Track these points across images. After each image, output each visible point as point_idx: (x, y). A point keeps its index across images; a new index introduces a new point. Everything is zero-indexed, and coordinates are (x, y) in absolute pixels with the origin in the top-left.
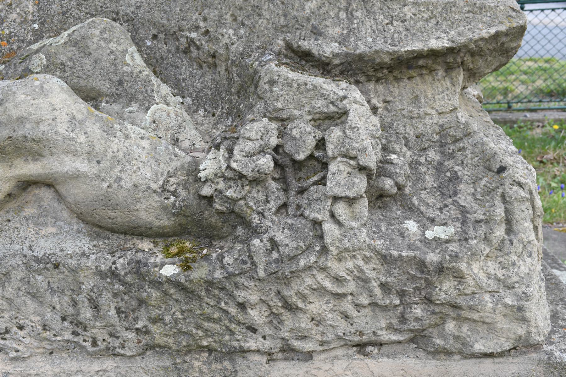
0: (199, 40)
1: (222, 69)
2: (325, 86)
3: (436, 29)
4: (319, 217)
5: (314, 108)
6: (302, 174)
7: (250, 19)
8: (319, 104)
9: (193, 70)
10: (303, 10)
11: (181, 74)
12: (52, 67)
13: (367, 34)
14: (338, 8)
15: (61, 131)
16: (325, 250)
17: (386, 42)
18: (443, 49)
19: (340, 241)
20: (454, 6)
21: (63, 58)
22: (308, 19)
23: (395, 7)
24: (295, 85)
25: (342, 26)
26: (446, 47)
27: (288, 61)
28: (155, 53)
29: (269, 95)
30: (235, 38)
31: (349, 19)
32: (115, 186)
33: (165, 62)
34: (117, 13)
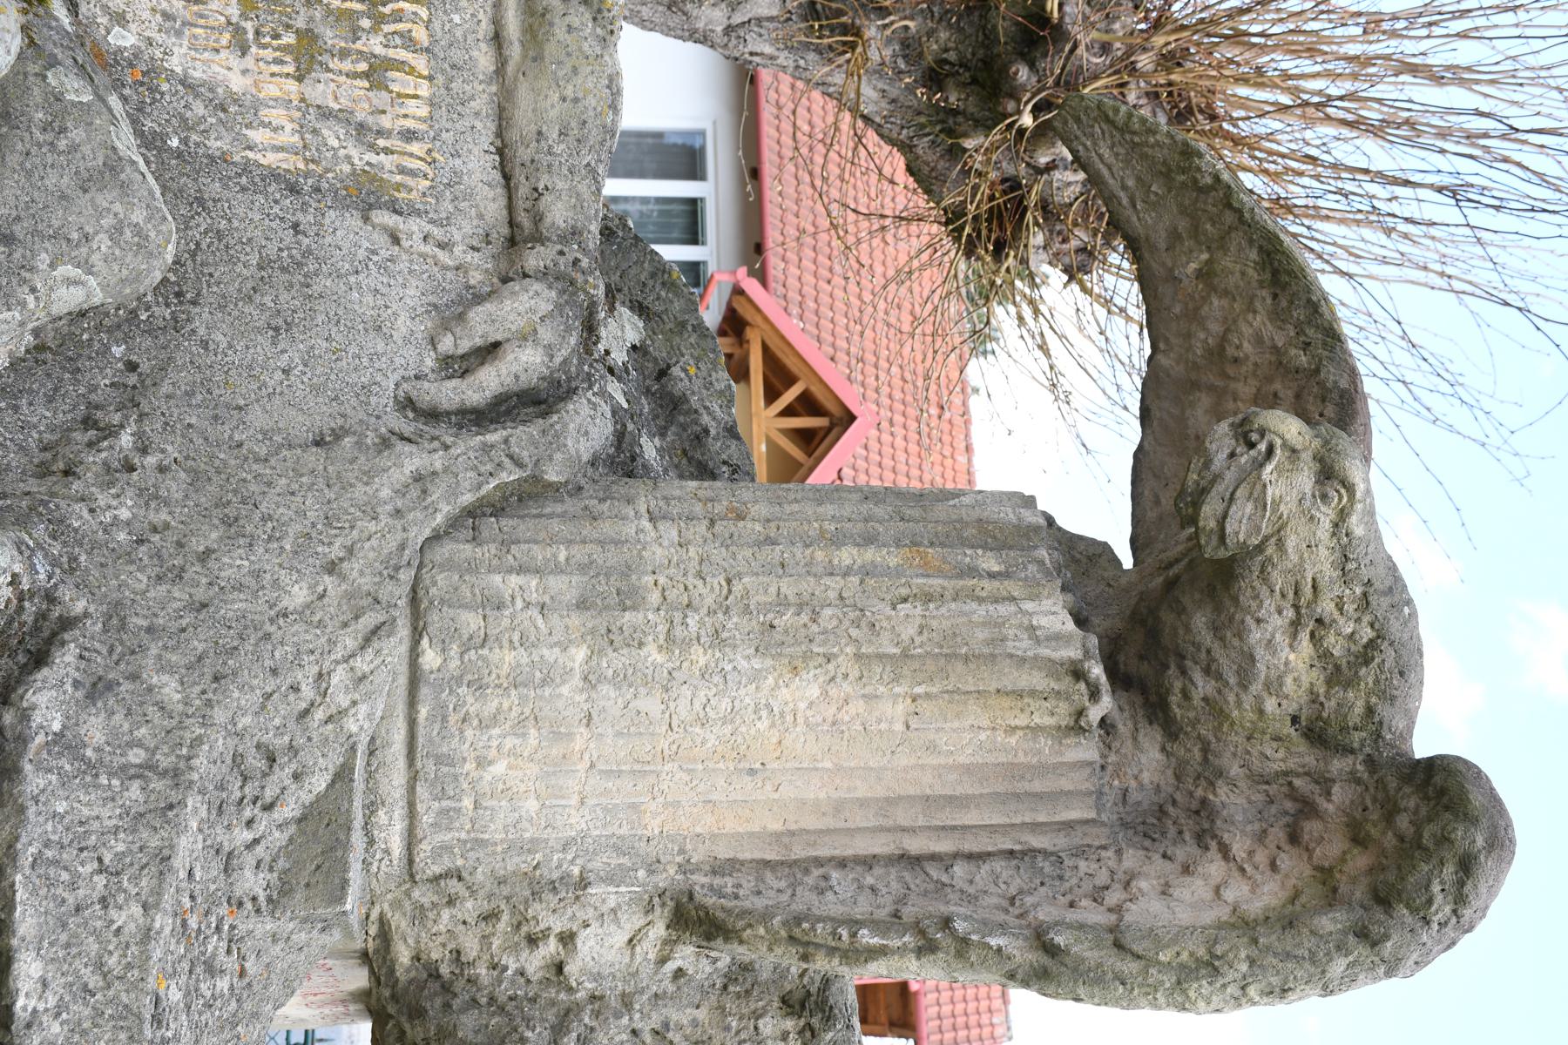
0: (111, 447)
1: (32, 485)
3: (71, 985)
7: (151, 557)
9: (40, 433)
10: (161, 670)
11: (31, 404)
12: (57, 107)
13: (75, 805)
14: (157, 748)
17: (47, 844)
18: (9, 993)
20: (131, 1038)
21: (77, 134)
22: (134, 677)
23: (144, 883)
25: (108, 749)
26: (13, 1003)
27: (28, 617)
28: (90, 358)
30: (107, 518)
31: (124, 768)
33: (67, 375)
34: (194, 303)
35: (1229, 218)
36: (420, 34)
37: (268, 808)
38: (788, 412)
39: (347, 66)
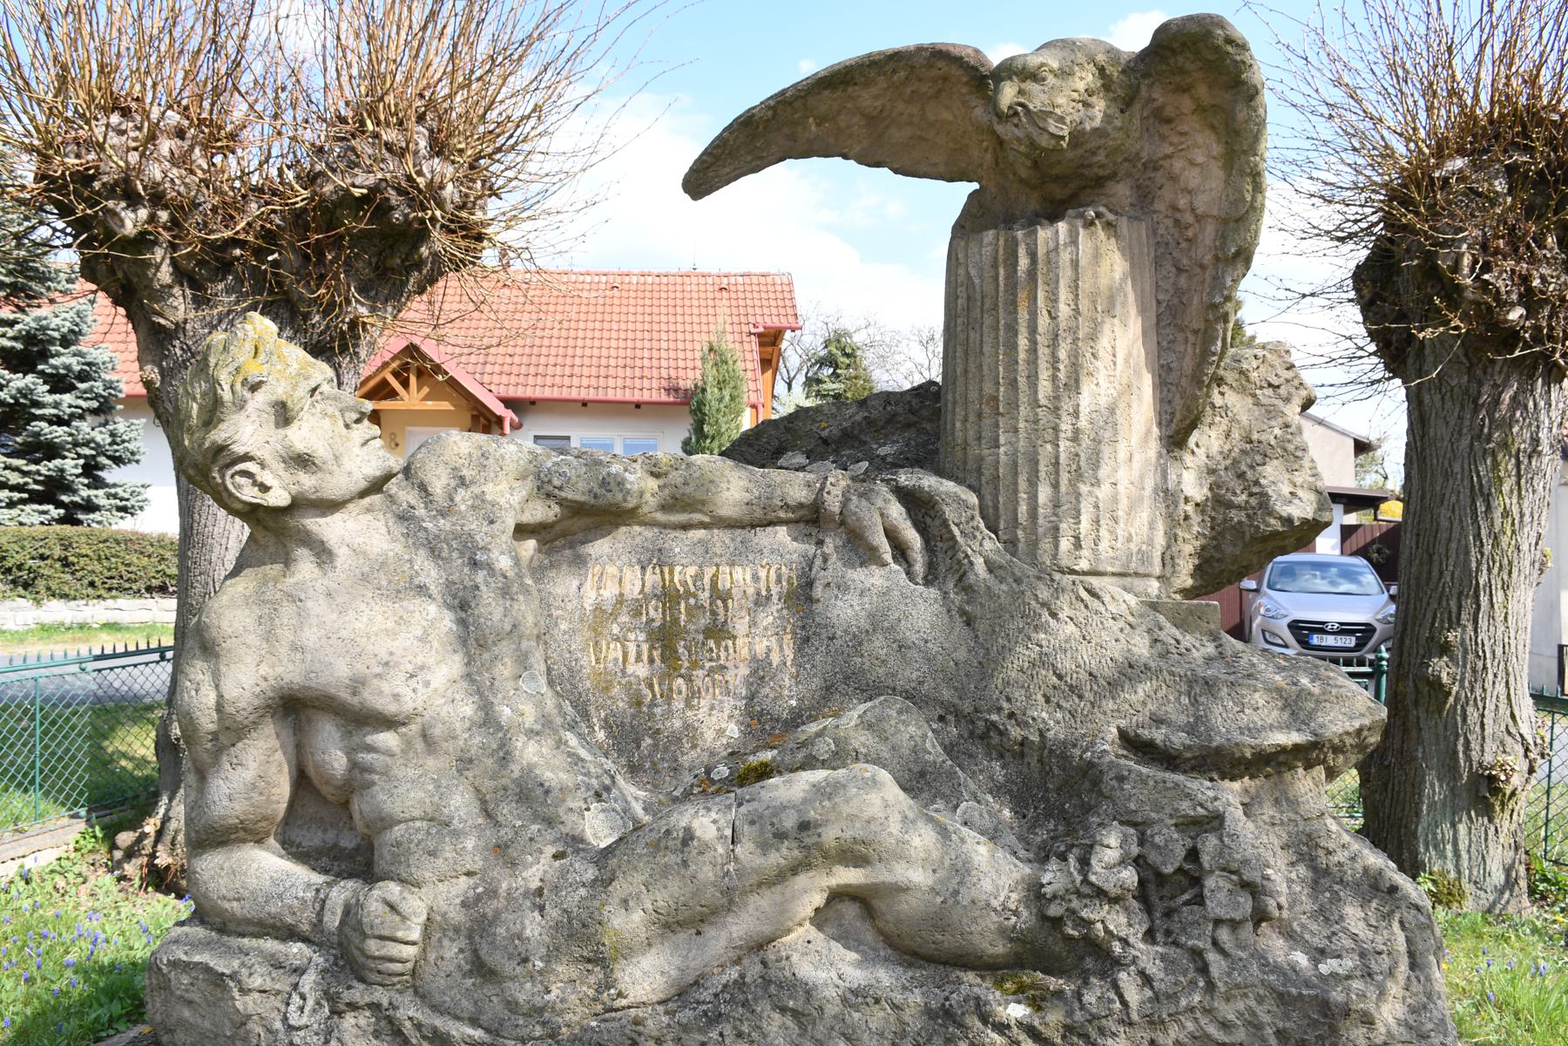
2: (1189, 784)
4: (1201, 944)
5: (1177, 810)
6: (1165, 891)
8: (1185, 806)
15: (895, 832)
16: (1211, 987)
19: (1229, 975)
24: (1151, 783)
29: (1118, 793)
32: (951, 902)
35: (798, 104)
36: (692, 570)
37: (1178, 642)
38: (405, 384)
39: (721, 611)
